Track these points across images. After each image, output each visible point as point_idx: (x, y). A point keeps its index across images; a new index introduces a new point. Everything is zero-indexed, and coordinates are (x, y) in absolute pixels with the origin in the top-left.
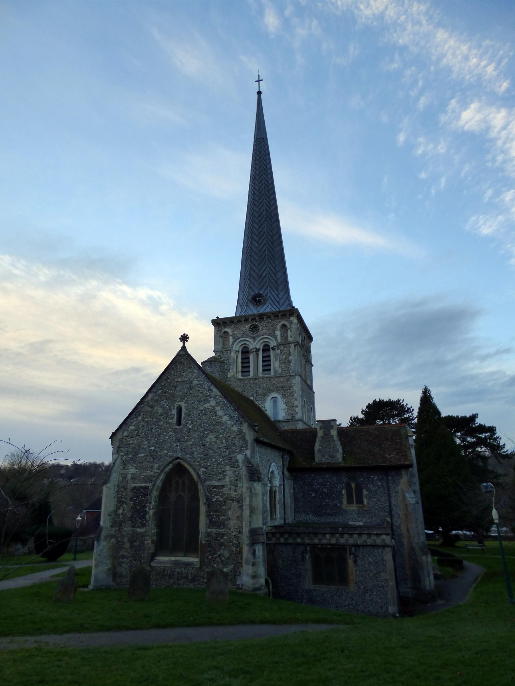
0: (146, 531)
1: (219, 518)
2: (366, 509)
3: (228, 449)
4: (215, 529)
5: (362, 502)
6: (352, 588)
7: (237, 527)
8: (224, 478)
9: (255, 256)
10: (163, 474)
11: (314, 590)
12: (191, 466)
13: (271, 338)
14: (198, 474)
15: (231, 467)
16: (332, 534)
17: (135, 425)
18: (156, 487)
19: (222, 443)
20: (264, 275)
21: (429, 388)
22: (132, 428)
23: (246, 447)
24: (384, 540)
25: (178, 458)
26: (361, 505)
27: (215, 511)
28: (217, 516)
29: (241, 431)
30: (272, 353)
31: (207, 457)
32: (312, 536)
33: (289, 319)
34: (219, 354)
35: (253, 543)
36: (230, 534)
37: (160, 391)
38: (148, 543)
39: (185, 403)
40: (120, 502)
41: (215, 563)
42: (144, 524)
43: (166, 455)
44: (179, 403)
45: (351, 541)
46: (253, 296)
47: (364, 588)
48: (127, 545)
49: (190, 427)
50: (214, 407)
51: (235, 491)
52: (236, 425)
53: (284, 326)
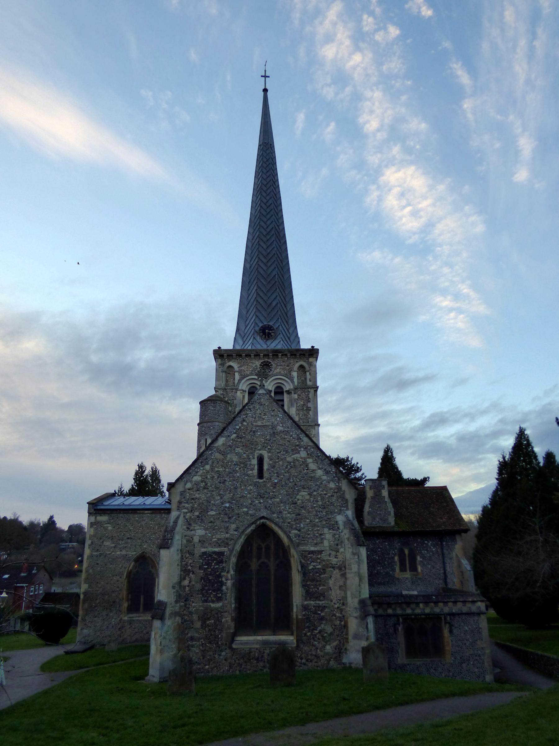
0: (223, 606)
1: (318, 589)
2: (420, 576)
3: (324, 508)
4: (313, 601)
5: (415, 569)
6: (449, 659)
7: (340, 598)
8: (322, 543)
9: (262, 280)
10: (243, 537)
11: (408, 664)
12: (280, 527)
13: (286, 379)
14: (289, 537)
15: (330, 529)
16: (426, 603)
17: (201, 476)
18: (234, 552)
19: (318, 501)
20: (274, 304)
21: (391, 447)
22: (197, 478)
23: (347, 507)
24: (479, 607)
25: (263, 517)
26: (415, 573)
27: (313, 580)
28: (315, 586)
29: (339, 488)
30: (286, 397)
31: (299, 518)
32: (404, 606)
33: (308, 359)
34: (221, 392)
35: (364, 616)
36: (333, 606)
37: (235, 435)
38: (227, 621)
39: (269, 452)
40: (185, 571)
41: (315, 641)
42: (220, 597)
43: (247, 513)
44: (261, 452)
45: (446, 610)
46: (262, 327)
47: (461, 658)
48: (198, 624)
49: (276, 481)
50: (304, 458)
51: (336, 557)
52: (333, 481)
53: (301, 367)
